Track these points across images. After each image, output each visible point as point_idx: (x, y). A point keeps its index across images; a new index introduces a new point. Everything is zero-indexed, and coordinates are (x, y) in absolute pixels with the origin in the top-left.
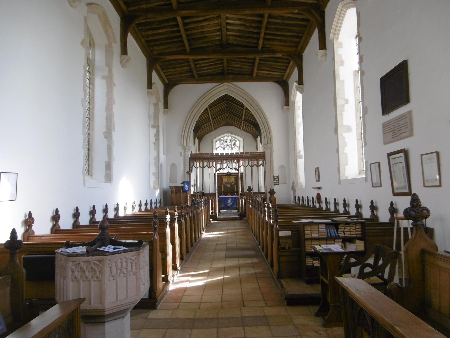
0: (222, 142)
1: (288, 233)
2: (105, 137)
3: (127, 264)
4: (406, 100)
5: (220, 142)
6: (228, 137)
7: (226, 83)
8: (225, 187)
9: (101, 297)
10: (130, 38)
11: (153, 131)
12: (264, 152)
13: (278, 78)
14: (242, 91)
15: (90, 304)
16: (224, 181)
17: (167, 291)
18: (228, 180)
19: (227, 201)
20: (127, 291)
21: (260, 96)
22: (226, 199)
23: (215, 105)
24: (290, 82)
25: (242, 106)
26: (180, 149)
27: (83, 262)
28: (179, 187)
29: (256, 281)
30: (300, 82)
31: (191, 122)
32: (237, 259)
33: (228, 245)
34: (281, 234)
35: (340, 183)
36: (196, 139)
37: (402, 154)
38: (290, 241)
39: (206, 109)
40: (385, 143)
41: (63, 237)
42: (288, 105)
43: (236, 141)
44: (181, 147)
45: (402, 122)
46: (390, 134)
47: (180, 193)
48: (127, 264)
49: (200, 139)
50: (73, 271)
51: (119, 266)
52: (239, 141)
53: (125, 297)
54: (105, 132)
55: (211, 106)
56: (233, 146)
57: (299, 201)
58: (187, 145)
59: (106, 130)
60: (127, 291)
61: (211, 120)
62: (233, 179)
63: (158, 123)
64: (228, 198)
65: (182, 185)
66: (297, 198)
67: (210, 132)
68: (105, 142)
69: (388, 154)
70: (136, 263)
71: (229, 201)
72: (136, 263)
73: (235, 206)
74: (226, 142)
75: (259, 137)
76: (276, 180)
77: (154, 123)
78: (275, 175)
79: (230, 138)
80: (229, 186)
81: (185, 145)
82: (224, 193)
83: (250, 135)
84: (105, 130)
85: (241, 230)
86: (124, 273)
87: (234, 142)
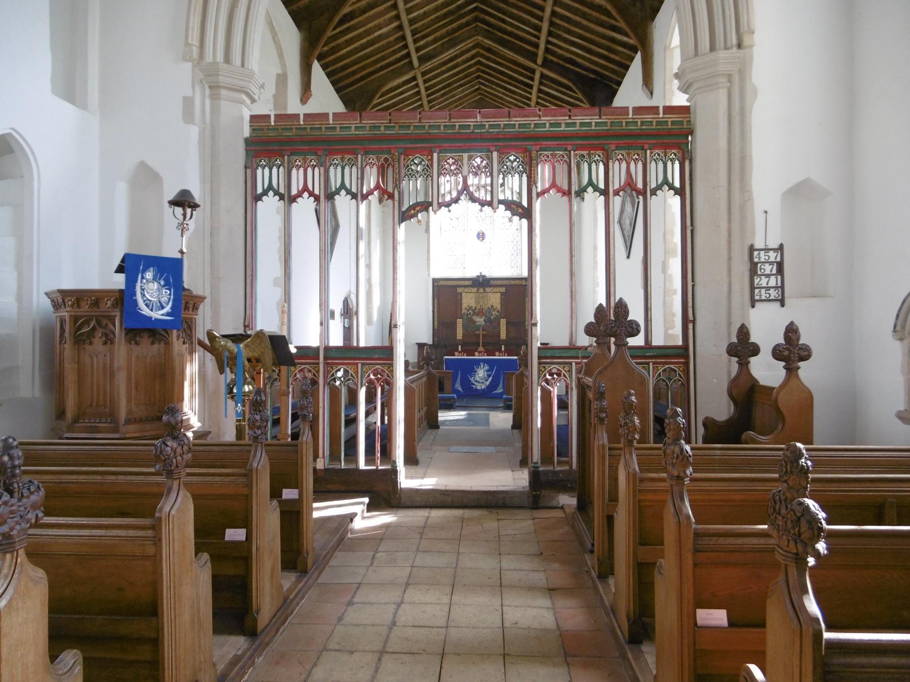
8: (469, 324)
10: (316, 67)
16: (465, 305)
18: (477, 302)
19: (473, 372)
22: (469, 368)
26: (181, 77)
28: (94, 298)
41: (99, 435)
44: (188, 66)
47: (109, 339)
58: (227, 60)
62: (494, 299)
64: (478, 362)
65: (119, 281)
71: (481, 373)
73: (500, 390)
76: (765, 272)
78: (759, 244)
80: (480, 320)
81: (215, 52)
82: (505, 342)
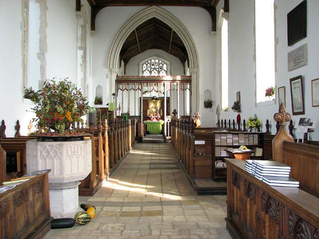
0: (149, 65)
1: (203, 142)
2: (38, 58)
3: (78, 149)
4: (304, 35)
5: (147, 65)
6: (155, 60)
7: (154, 7)
9: (62, 172)
11: (80, 53)
12: (191, 76)
13: (205, 3)
14: (170, 14)
15: (54, 174)
17: (100, 187)
20: (78, 168)
21: (188, 21)
23: (143, 28)
24: (217, 8)
25: (170, 29)
27: (48, 145)
29: (174, 183)
30: (226, 9)
31: (118, 45)
32: (160, 170)
33: (152, 161)
34: (197, 142)
35: (256, 106)
36: (122, 61)
37: (300, 80)
38: (204, 150)
39: (134, 31)
40: (290, 70)
42: (215, 31)
43: (163, 65)
45: (301, 53)
46: (293, 62)
48: (78, 149)
49: (126, 62)
50: (41, 152)
51: (73, 150)
52: (166, 65)
53: (77, 172)
54: (38, 53)
55: (137, 29)
56: (160, 70)
57: (230, 125)
59: (39, 52)
60: (78, 168)
61: (138, 43)
63: (85, 45)
66: (220, 121)
67: (137, 54)
68: (38, 63)
69: (290, 79)
70: (84, 149)
72: (84, 149)
74: (153, 65)
75: (186, 61)
77: (81, 44)
79: (157, 61)
81: (111, 67)
83: (178, 59)
84: (38, 51)
85: (165, 150)
86: (76, 155)
87: (161, 65)
